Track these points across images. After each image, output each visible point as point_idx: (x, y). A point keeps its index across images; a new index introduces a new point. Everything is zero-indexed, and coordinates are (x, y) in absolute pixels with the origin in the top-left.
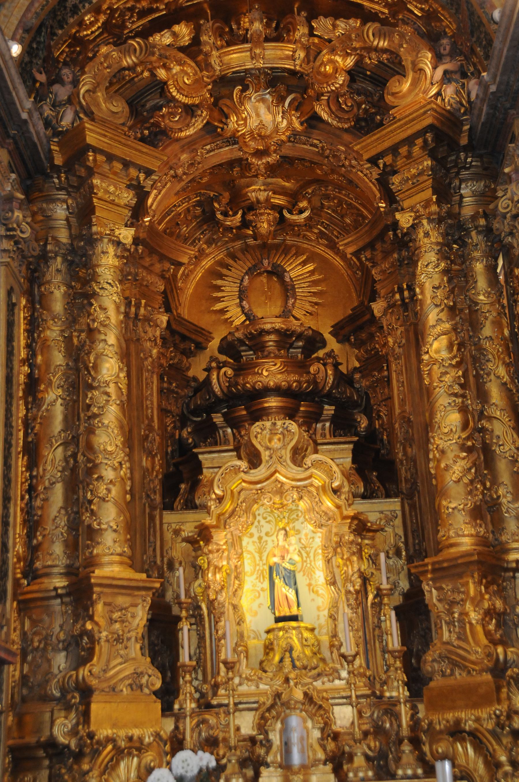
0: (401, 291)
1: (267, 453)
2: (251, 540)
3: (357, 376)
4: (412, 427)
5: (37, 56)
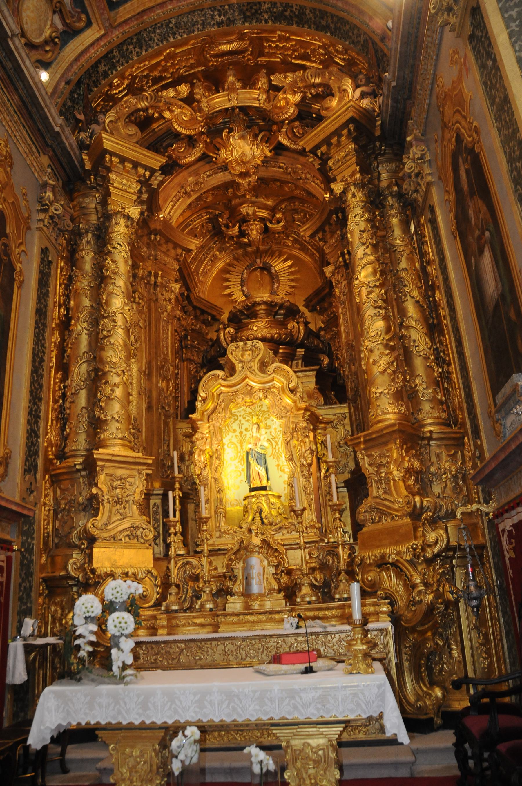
0: (343, 255)
1: (240, 365)
2: (234, 434)
3: (322, 333)
4: (354, 351)
5: (77, 104)
